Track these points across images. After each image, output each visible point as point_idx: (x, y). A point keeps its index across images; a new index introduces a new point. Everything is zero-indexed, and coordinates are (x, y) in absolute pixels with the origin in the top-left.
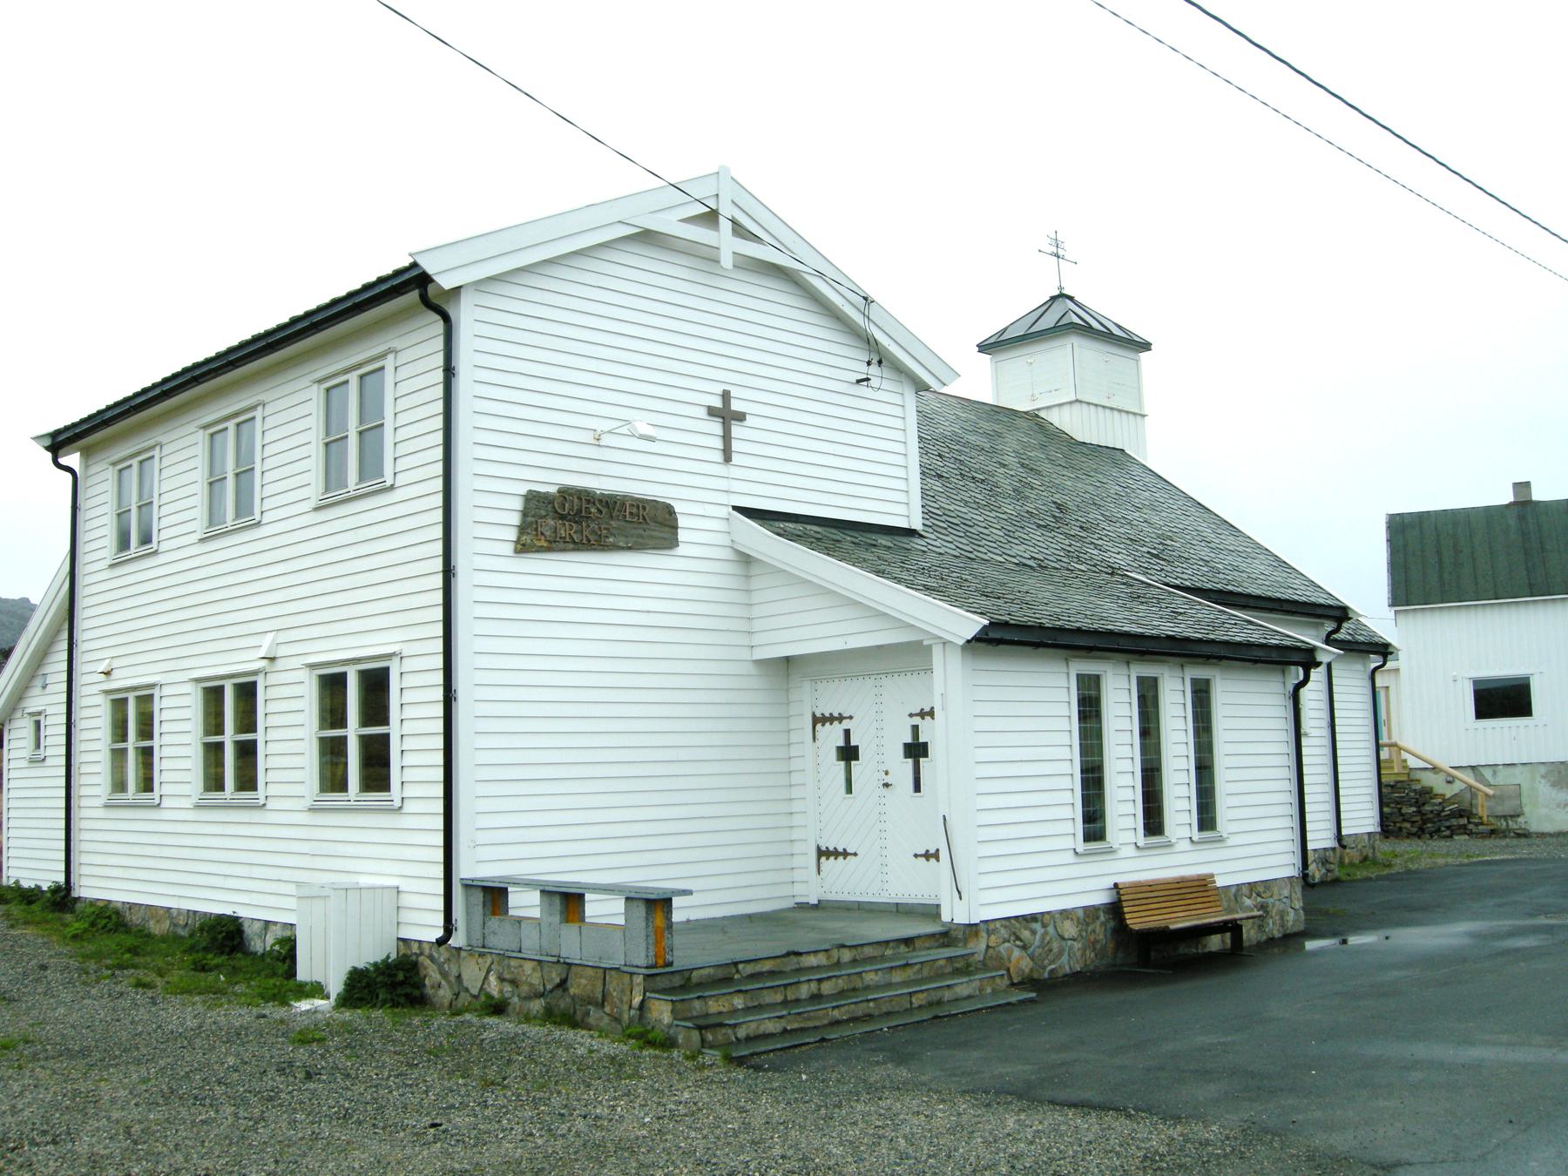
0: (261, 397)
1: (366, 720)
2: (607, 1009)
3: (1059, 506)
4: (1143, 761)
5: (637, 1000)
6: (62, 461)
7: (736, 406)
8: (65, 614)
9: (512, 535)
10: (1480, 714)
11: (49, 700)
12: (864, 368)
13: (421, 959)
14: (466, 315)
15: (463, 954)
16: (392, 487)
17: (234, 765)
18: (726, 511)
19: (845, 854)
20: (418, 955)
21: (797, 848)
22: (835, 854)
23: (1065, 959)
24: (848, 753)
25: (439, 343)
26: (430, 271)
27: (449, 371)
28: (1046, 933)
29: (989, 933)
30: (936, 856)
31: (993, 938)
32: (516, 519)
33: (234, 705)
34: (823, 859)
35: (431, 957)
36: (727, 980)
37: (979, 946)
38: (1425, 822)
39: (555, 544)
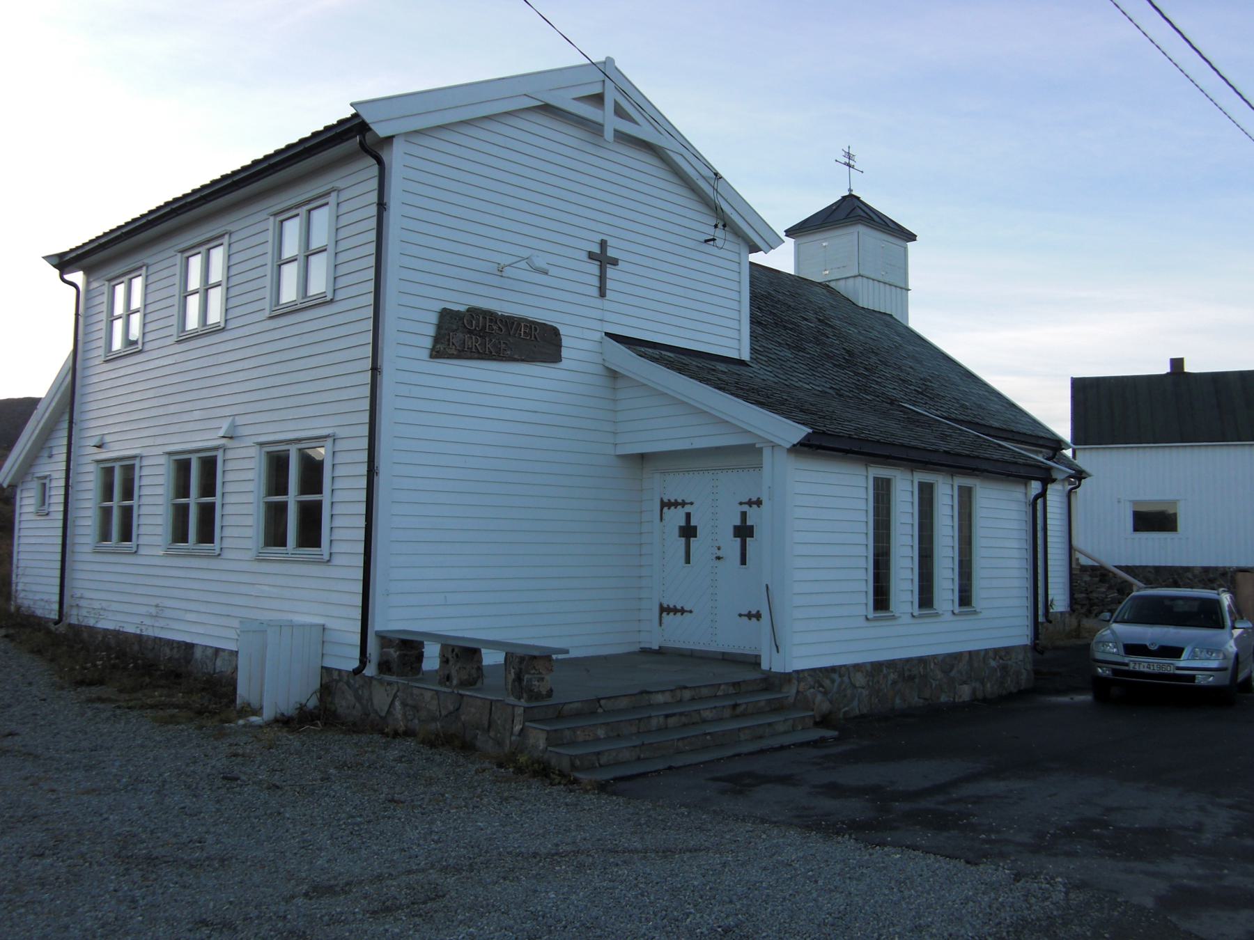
0: (229, 228)
1: (304, 490)
2: (492, 734)
3: (848, 352)
4: (920, 549)
5: (517, 728)
6: (67, 277)
7: (611, 253)
8: (69, 400)
9: (428, 343)
10: (1136, 529)
11: (54, 468)
12: (711, 231)
13: (340, 684)
14: (397, 157)
15: (374, 682)
16: (332, 301)
17: (196, 524)
19: (683, 611)
20: (337, 681)
22: (675, 610)
23: (855, 703)
25: (374, 184)
26: (368, 121)
27: (382, 206)
28: (842, 682)
29: (799, 680)
30: (758, 616)
31: (802, 684)
32: (431, 331)
33: (198, 475)
34: (664, 614)
35: (348, 683)
36: (593, 713)
37: (791, 691)
38: (1092, 605)
39: (463, 353)
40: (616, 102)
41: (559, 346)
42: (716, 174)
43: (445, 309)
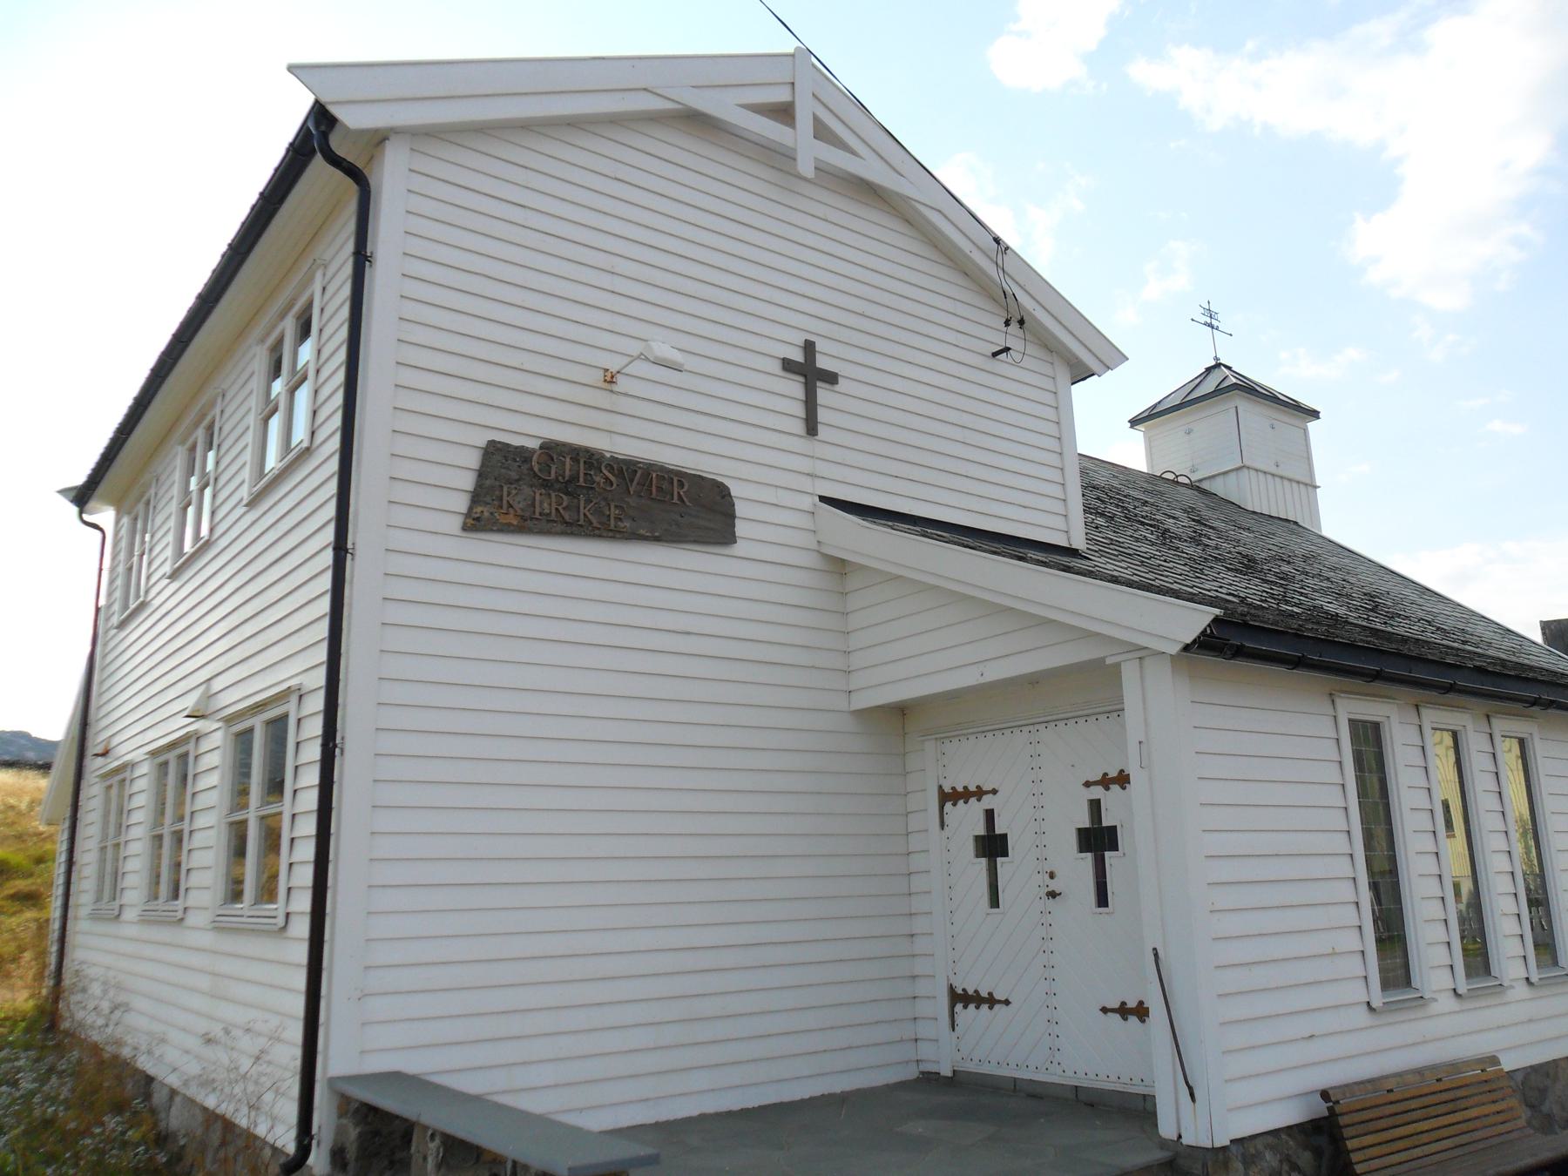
6: (85, 517)
7: (822, 363)
9: (461, 503)
14: (393, 177)
18: (808, 502)
19: (991, 1001)
21: (922, 988)
24: (992, 846)
30: (1141, 1012)
32: (468, 481)
39: (528, 524)
40: (816, 119)
41: (730, 516)
42: (997, 240)
43: (492, 443)
